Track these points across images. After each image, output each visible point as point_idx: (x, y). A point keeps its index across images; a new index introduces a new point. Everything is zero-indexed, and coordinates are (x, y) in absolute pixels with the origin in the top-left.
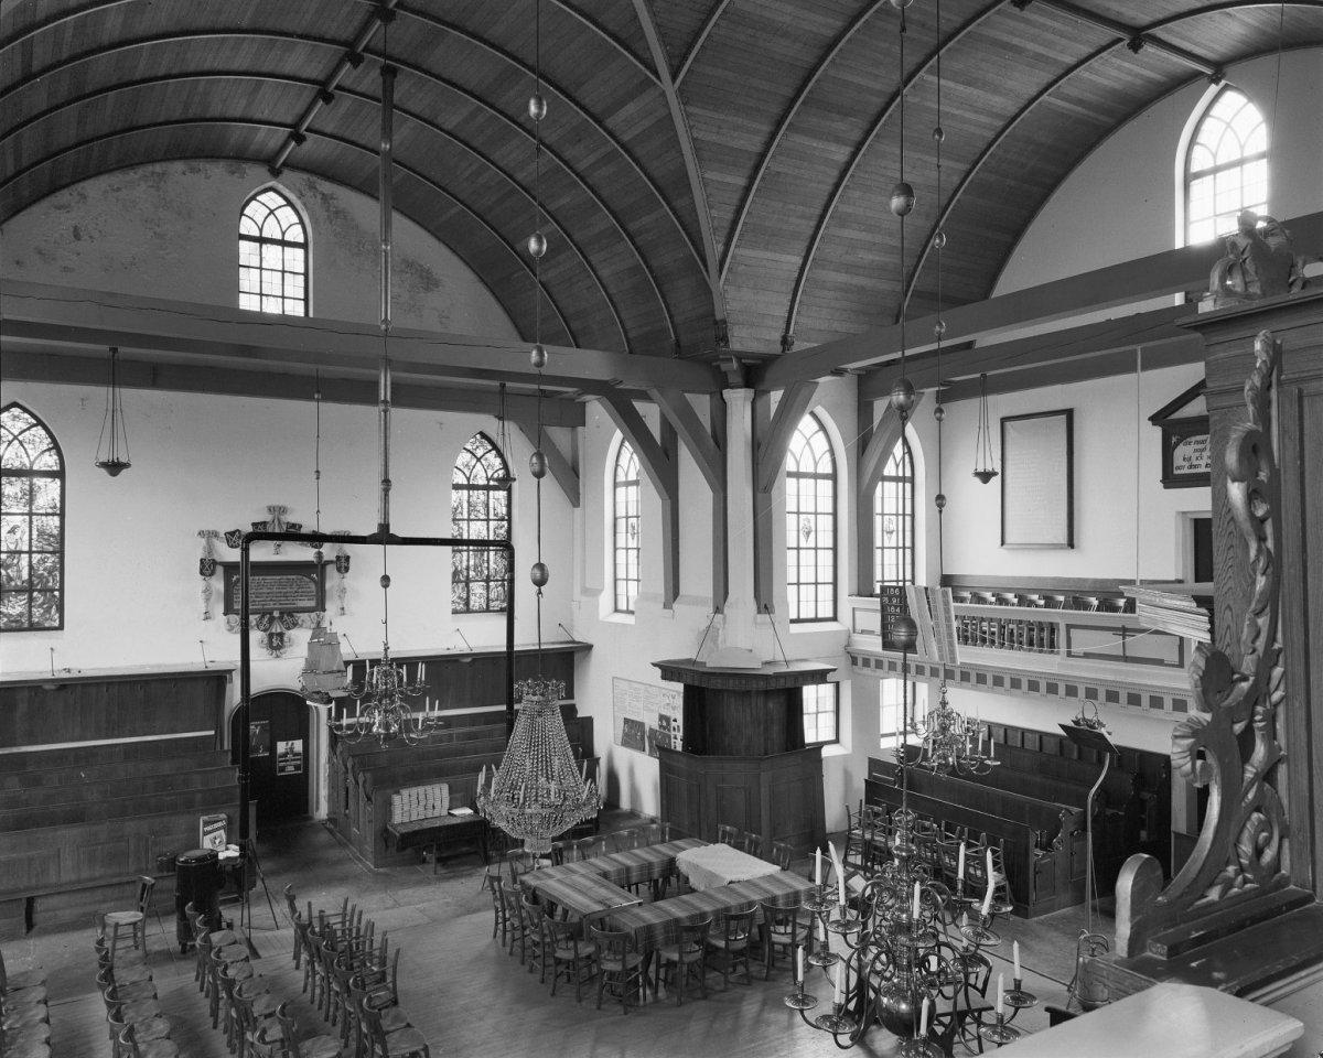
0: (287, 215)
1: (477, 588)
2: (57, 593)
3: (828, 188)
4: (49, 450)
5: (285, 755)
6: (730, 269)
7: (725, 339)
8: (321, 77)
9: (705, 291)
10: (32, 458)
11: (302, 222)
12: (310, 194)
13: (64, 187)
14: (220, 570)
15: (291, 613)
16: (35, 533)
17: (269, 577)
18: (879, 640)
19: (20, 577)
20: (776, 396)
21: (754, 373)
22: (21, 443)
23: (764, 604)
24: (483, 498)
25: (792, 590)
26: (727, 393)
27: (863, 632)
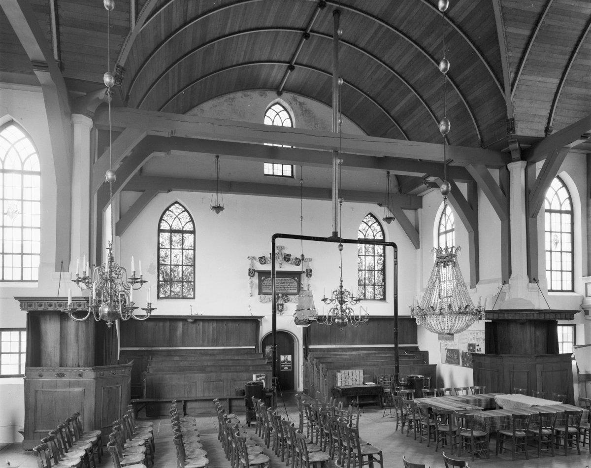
0: (284, 115)
1: (369, 288)
2: (192, 283)
3: (579, 33)
4: (190, 222)
5: (284, 362)
6: (517, 88)
7: (513, 129)
8: (304, 26)
9: (502, 103)
10: (183, 225)
11: (290, 118)
12: (294, 103)
13: (195, 106)
14: (257, 274)
15: (286, 295)
16: (184, 257)
17: (278, 279)
19: (178, 276)
20: (540, 165)
21: (528, 150)
22: (179, 219)
23: (533, 276)
25: (548, 274)
26: (510, 166)
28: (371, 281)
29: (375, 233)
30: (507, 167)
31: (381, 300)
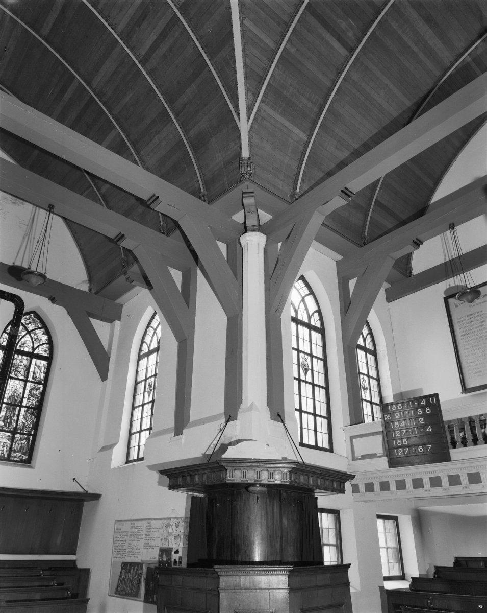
18: (385, 460)
24: (25, 362)
27: (364, 457)
28: (10, 423)
29: (36, 345)
30: (239, 239)
31: (22, 461)
